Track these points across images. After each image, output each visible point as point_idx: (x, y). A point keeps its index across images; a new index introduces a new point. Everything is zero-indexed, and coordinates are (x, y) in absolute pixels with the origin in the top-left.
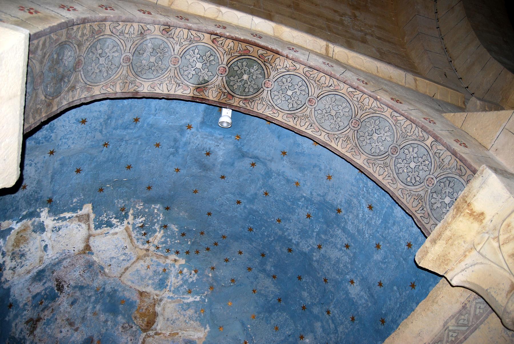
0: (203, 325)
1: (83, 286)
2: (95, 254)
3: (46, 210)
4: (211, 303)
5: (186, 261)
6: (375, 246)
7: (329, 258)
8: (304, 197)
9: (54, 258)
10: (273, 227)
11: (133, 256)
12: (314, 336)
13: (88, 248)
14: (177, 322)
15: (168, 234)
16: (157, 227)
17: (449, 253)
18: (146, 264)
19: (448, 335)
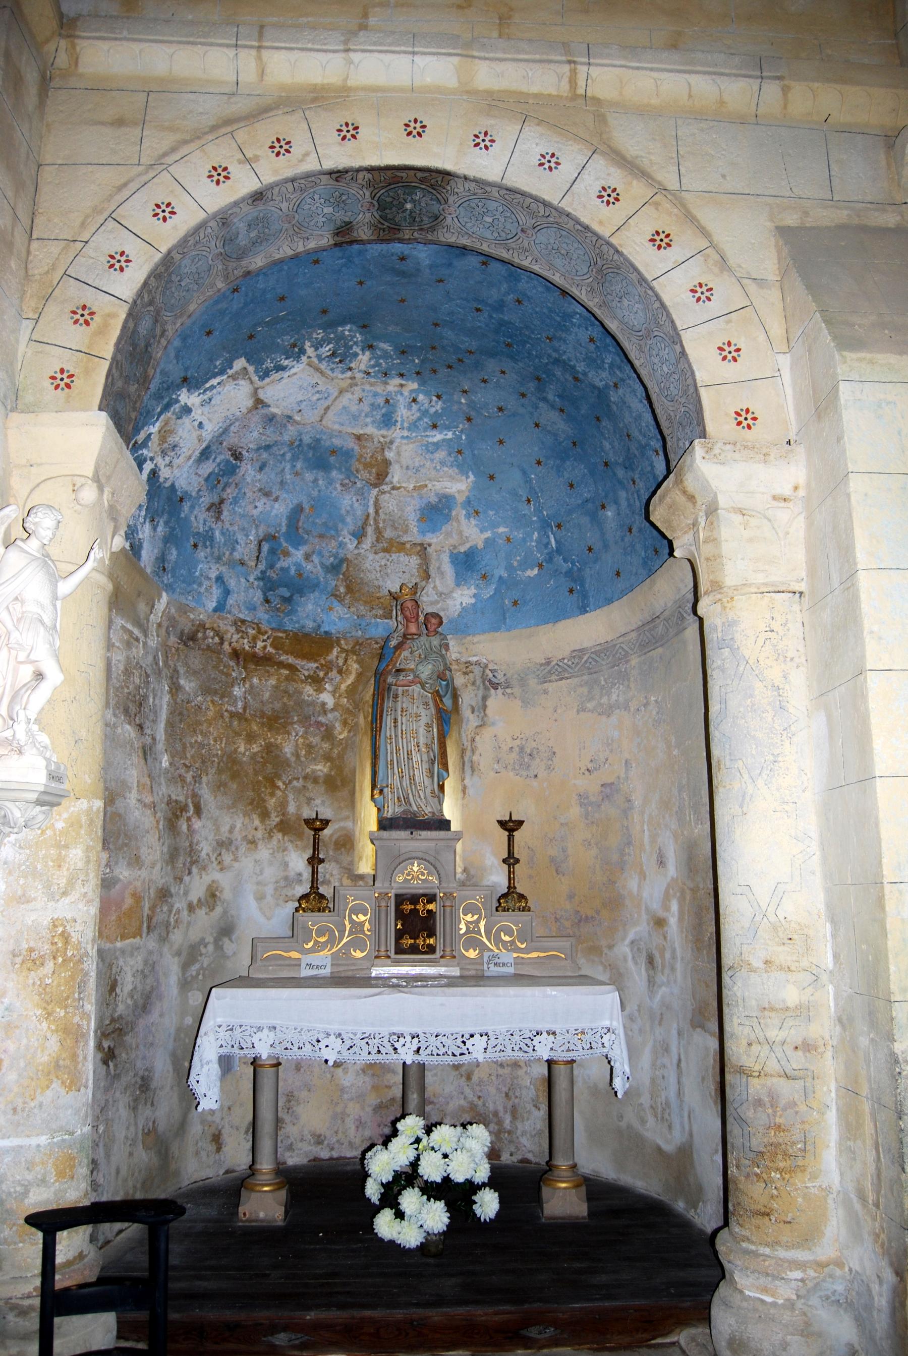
0: (463, 469)
3: (184, 390)
13: (259, 403)
16: (356, 349)
18: (356, 396)
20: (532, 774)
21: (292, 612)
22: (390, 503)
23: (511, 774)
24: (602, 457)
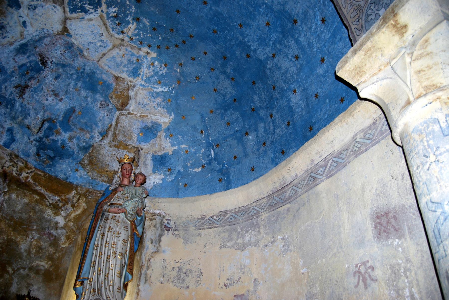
0: (169, 112)
1: (65, 64)
2: (73, 37)
4: (177, 95)
5: (157, 55)
6: (320, 59)
7: (280, 67)
8: (266, 4)
9: (34, 34)
10: (235, 31)
11: (109, 44)
12: (257, 134)
13: (65, 31)
14: (147, 107)
15: (140, 27)
16: (130, 19)
17: (365, 65)
19: (354, 145)
20: (185, 286)
21: (53, 166)
22: (125, 121)
23: (171, 285)
24: (251, 106)
